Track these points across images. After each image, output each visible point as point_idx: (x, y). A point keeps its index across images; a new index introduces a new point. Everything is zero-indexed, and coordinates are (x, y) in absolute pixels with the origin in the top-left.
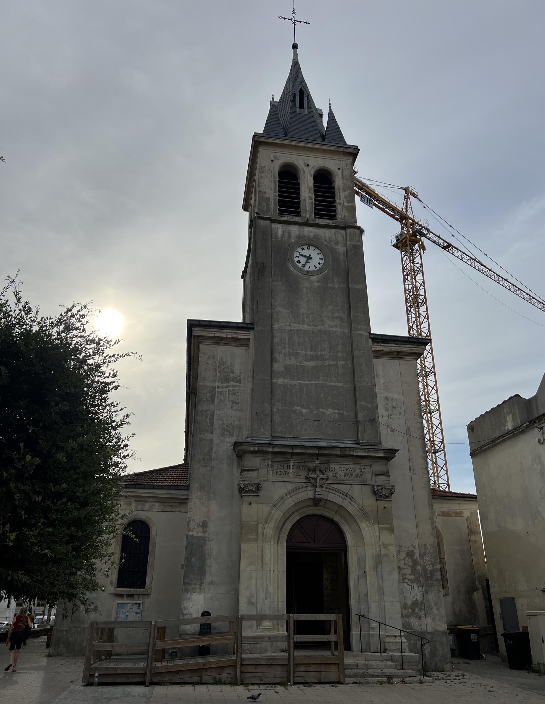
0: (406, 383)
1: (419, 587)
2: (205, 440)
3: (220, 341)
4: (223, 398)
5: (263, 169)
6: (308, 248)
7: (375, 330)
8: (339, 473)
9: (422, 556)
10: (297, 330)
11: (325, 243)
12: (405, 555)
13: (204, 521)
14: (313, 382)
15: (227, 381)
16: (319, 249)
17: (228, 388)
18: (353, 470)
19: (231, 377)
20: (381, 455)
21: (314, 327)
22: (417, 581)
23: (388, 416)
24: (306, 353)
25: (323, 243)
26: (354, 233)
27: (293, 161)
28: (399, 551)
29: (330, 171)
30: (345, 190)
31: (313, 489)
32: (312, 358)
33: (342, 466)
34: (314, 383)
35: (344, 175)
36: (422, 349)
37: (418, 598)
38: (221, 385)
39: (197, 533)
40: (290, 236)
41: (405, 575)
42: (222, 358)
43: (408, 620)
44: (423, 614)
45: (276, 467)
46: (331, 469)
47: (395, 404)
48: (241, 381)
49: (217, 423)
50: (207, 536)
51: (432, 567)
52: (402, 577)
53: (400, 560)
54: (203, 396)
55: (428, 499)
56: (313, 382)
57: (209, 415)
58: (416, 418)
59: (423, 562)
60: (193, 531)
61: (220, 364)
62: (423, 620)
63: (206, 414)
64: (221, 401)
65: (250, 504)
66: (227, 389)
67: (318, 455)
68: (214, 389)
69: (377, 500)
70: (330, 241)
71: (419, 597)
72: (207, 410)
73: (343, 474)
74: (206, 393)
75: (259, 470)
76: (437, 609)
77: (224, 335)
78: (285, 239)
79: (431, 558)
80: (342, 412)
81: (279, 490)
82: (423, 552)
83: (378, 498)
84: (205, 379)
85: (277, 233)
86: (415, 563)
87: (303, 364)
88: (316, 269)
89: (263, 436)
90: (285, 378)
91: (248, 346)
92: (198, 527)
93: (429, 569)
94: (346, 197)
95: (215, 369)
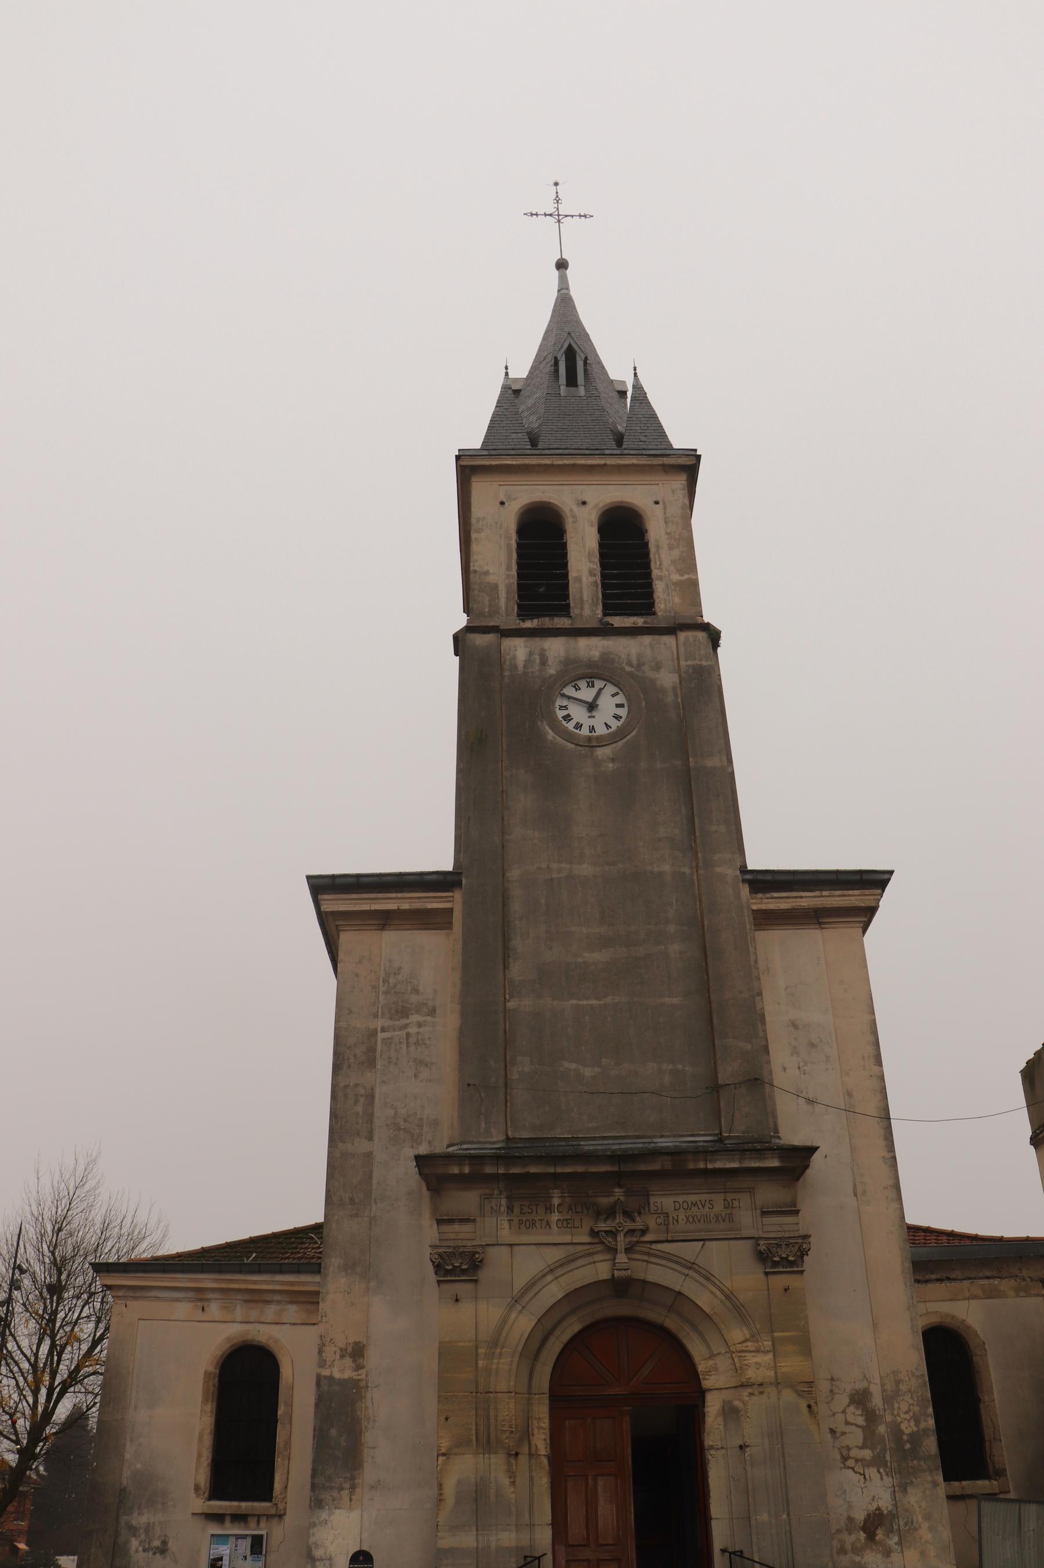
1: (885, 1477)
3: (385, 920)
5: (480, 523)
6: (588, 685)
7: (755, 861)
8: (673, 1214)
9: (889, 1400)
11: (628, 669)
12: (848, 1401)
14: (609, 1000)
15: (403, 1012)
16: (615, 685)
17: (406, 1030)
18: (707, 1205)
19: (412, 1004)
20: (775, 1163)
22: (878, 1462)
25: (623, 669)
26: (695, 641)
28: (831, 1391)
29: (636, 509)
30: (671, 548)
31: (608, 1257)
33: (680, 1199)
35: (668, 515)
36: (872, 897)
37: (881, 1504)
39: (342, 1371)
40: (544, 662)
41: (849, 1449)
42: (390, 961)
43: (858, 1559)
44: (896, 1544)
45: (517, 1210)
46: (653, 1208)
48: (438, 1012)
49: (381, 1114)
50: (363, 1377)
51: (915, 1425)
52: (841, 1454)
53: (834, 1414)
55: (902, 1262)
56: (609, 1000)
57: (362, 1096)
59: (892, 1414)
60: (332, 1366)
62: (895, 1557)
64: (389, 1062)
65: (457, 1300)
66: (403, 1033)
67: (617, 1179)
68: (374, 1033)
69: (767, 1274)
70: (640, 665)
71: (885, 1502)
72: (356, 1085)
73: (682, 1216)
75: (478, 1219)
77: (392, 906)
79: (913, 1405)
80: (680, 1066)
83: (771, 1268)
85: (514, 658)
86: (871, 1417)
89: (486, 1140)
91: (448, 925)
92: (342, 1357)
94: (673, 562)
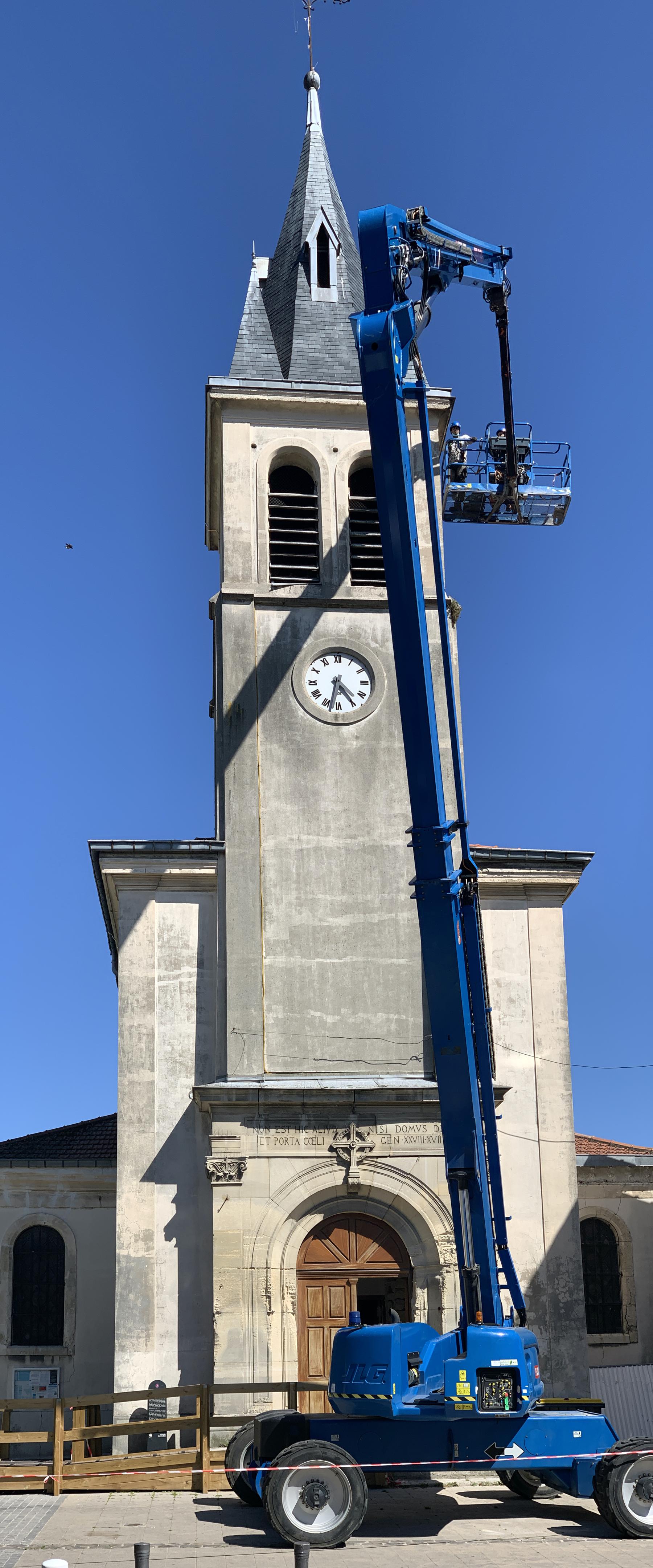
0: (540, 948)
2: (140, 1084)
4: (169, 1000)
5: (233, 470)
8: (394, 1135)
10: (317, 849)
11: (373, 645)
13: (146, 1230)
14: (348, 959)
17: (179, 980)
19: (183, 957)
21: (349, 841)
23: (499, 1019)
24: (333, 898)
27: (302, 441)
32: (346, 909)
34: (349, 961)
38: (164, 973)
39: (136, 1251)
42: (163, 918)
44: (548, 1378)
47: (513, 995)
54: (131, 997)
55: (570, 1176)
57: (145, 1034)
58: (555, 1020)
59: (553, 1288)
61: (162, 931)
63: (140, 1034)
66: (176, 982)
72: (139, 1026)
73: (402, 1137)
74: (137, 992)
76: (574, 1368)
78: (285, 642)
79: (569, 1282)
80: (404, 1017)
81: (284, 1171)
82: (554, 1272)
84: (132, 963)
87: (328, 924)
88: (355, 708)
90: (290, 955)
92: (136, 1241)
93: (564, 1301)
95: (151, 942)
